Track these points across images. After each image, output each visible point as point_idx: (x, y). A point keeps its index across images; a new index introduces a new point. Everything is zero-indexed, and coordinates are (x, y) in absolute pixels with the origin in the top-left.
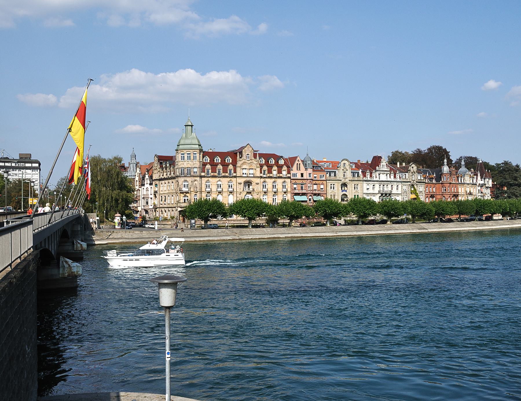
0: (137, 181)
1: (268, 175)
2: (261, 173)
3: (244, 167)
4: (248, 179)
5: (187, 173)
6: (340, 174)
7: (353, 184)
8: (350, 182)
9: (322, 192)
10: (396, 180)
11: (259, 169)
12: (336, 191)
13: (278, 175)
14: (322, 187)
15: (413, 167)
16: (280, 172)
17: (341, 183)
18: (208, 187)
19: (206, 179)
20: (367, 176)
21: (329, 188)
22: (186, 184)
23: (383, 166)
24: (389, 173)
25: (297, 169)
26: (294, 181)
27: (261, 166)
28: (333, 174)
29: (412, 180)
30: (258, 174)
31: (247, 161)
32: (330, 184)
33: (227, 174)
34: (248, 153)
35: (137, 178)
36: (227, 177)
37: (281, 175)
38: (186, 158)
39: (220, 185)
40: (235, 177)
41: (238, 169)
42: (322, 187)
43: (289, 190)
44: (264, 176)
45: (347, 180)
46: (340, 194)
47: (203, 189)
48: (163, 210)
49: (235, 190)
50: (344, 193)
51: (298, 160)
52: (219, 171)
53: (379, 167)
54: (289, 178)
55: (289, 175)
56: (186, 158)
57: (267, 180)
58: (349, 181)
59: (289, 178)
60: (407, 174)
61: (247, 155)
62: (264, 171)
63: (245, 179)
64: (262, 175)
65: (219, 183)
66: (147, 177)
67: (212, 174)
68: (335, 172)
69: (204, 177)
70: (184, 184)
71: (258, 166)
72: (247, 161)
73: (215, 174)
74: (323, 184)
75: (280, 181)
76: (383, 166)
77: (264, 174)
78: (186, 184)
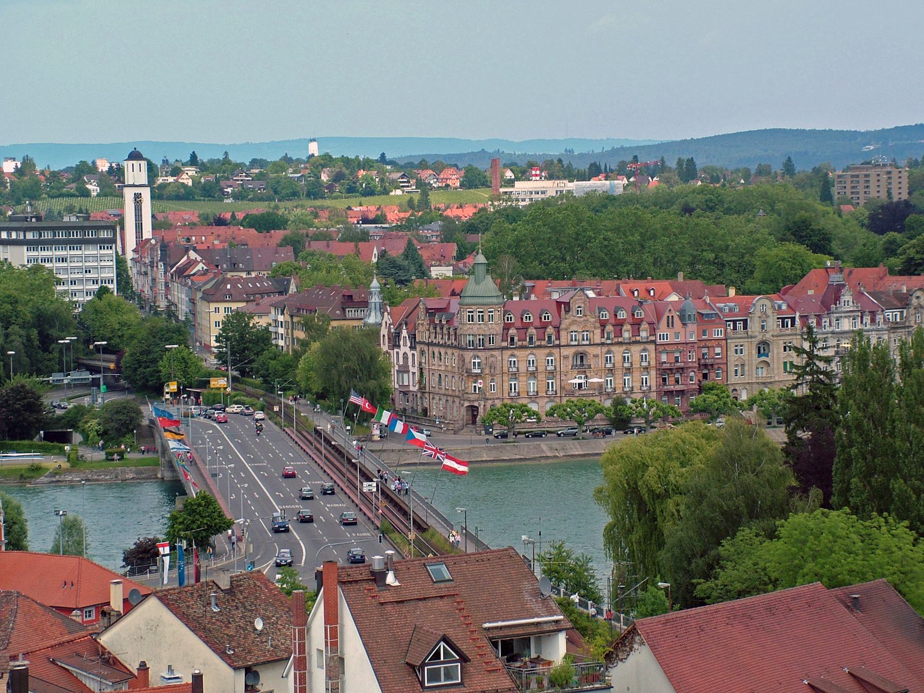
0: (384, 336)
1: (616, 340)
2: (603, 337)
3: (574, 328)
4: (581, 349)
5: (482, 344)
6: (754, 326)
7: (781, 342)
8: (775, 338)
9: (717, 361)
10: (875, 327)
11: (598, 332)
12: (746, 358)
13: (633, 339)
14: (718, 350)
15: (918, 298)
16: (636, 332)
17: (755, 341)
18: (513, 366)
19: (509, 352)
20: (823, 324)
21: (731, 352)
22: (477, 361)
23: (846, 304)
24: (860, 314)
25: (668, 326)
26: (660, 348)
27: (603, 325)
28: (740, 325)
29: (915, 323)
30: (598, 339)
31: (578, 319)
32: (733, 345)
33: (543, 343)
34: (580, 305)
35: (384, 331)
36: (545, 347)
37: (638, 338)
38: (476, 318)
39: (533, 361)
40: (559, 346)
41: (563, 334)
42: (718, 350)
43: (653, 363)
44: (609, 342)
45: (768, 336)
46: (754, 362)
47: (505, 369)
48: (436, 350)
49: (558, 369)
50: (763, 358)
51: (670, 310)
52: (531, 338)
53: (836, 305)
54: (654, 342)
55: (653, 338)
56: (476, 318)
57: (613, 348)
58: (773, 336)
59: (654, 342)
60: (905, 311)
61: (579, 307)
62: (608, 334)
63: (573, 350)
64: (603, 340)
65: (531, 358)
66: (404, 333)
67: (520, 343)
68: (745, 322)
69: (506, 348)
70: (473, 361)
71: (598, 325)
72: (578, 319)
73: (524, 343)
74: (719, 346)
75: (636, 349)
76: (846, 304)
77: (608, 338)
78: (477, 361)
